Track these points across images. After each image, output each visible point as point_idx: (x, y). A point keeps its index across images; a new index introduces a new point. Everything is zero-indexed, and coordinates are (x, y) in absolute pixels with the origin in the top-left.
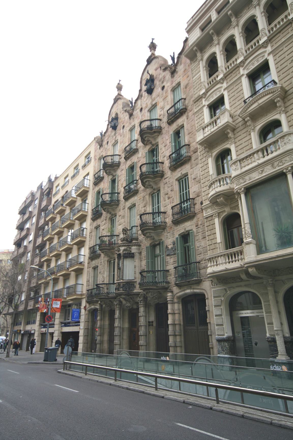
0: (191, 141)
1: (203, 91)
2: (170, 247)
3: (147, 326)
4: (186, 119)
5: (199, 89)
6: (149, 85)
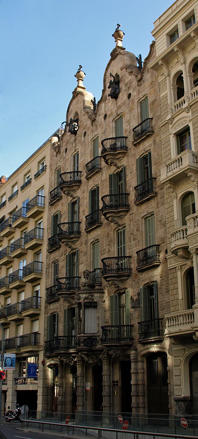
1: (169, 117)
3: (112, 385)
6: (114, 88)
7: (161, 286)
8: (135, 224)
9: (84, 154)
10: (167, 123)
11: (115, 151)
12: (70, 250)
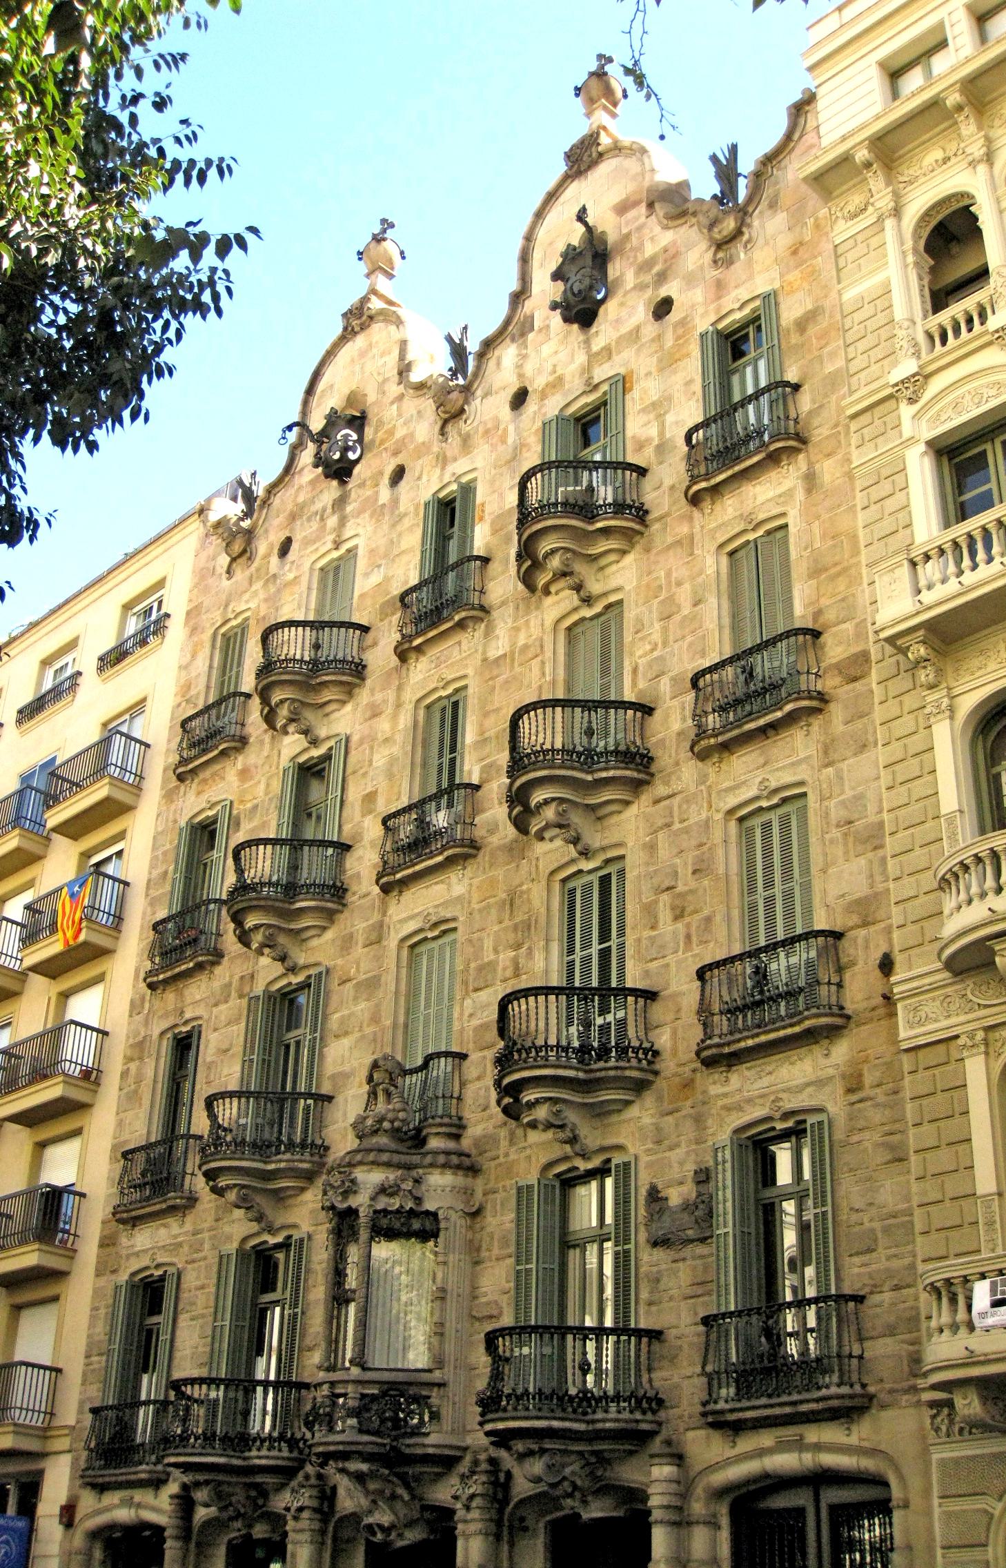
0: (830, 616)
2: (674, 1197)
4: (800, 495)
5: (878, 353)
7: (851, 1131)
8: (688, 842)
9: (386, 556)
10: (890, 397)
11: (592, 518)
12: (279, 968)
